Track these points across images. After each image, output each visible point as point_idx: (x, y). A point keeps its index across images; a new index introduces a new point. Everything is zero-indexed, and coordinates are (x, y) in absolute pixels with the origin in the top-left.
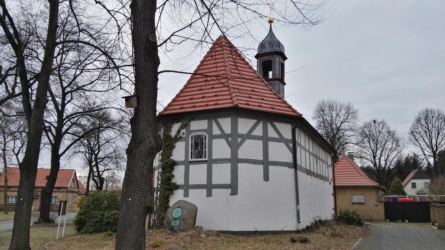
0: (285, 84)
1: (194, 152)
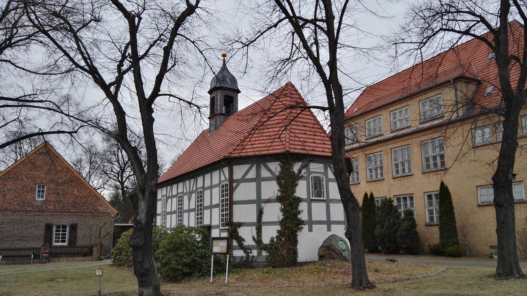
0: (238, 91)
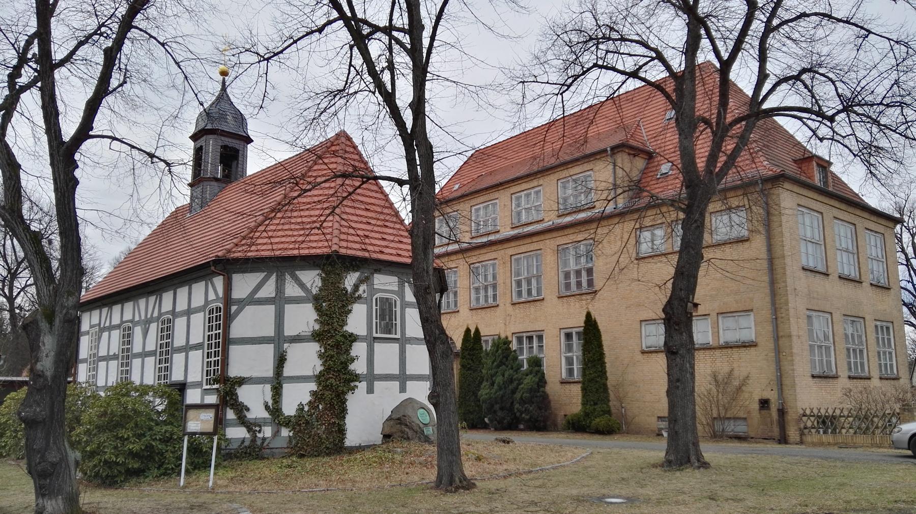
0: (249, 140)
1: (380, 323)
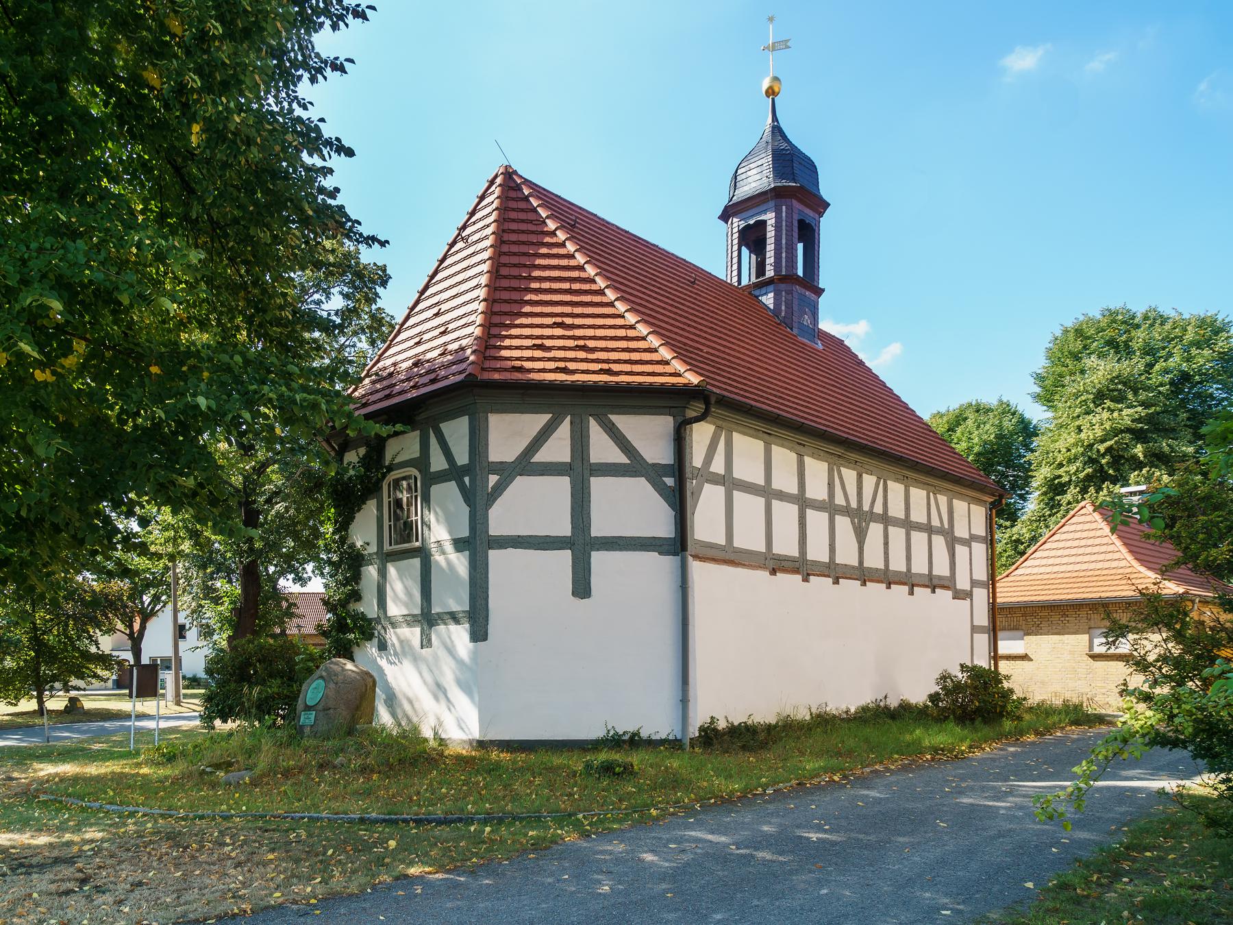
0: (819, 292)
1: (395, 525)
